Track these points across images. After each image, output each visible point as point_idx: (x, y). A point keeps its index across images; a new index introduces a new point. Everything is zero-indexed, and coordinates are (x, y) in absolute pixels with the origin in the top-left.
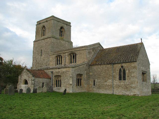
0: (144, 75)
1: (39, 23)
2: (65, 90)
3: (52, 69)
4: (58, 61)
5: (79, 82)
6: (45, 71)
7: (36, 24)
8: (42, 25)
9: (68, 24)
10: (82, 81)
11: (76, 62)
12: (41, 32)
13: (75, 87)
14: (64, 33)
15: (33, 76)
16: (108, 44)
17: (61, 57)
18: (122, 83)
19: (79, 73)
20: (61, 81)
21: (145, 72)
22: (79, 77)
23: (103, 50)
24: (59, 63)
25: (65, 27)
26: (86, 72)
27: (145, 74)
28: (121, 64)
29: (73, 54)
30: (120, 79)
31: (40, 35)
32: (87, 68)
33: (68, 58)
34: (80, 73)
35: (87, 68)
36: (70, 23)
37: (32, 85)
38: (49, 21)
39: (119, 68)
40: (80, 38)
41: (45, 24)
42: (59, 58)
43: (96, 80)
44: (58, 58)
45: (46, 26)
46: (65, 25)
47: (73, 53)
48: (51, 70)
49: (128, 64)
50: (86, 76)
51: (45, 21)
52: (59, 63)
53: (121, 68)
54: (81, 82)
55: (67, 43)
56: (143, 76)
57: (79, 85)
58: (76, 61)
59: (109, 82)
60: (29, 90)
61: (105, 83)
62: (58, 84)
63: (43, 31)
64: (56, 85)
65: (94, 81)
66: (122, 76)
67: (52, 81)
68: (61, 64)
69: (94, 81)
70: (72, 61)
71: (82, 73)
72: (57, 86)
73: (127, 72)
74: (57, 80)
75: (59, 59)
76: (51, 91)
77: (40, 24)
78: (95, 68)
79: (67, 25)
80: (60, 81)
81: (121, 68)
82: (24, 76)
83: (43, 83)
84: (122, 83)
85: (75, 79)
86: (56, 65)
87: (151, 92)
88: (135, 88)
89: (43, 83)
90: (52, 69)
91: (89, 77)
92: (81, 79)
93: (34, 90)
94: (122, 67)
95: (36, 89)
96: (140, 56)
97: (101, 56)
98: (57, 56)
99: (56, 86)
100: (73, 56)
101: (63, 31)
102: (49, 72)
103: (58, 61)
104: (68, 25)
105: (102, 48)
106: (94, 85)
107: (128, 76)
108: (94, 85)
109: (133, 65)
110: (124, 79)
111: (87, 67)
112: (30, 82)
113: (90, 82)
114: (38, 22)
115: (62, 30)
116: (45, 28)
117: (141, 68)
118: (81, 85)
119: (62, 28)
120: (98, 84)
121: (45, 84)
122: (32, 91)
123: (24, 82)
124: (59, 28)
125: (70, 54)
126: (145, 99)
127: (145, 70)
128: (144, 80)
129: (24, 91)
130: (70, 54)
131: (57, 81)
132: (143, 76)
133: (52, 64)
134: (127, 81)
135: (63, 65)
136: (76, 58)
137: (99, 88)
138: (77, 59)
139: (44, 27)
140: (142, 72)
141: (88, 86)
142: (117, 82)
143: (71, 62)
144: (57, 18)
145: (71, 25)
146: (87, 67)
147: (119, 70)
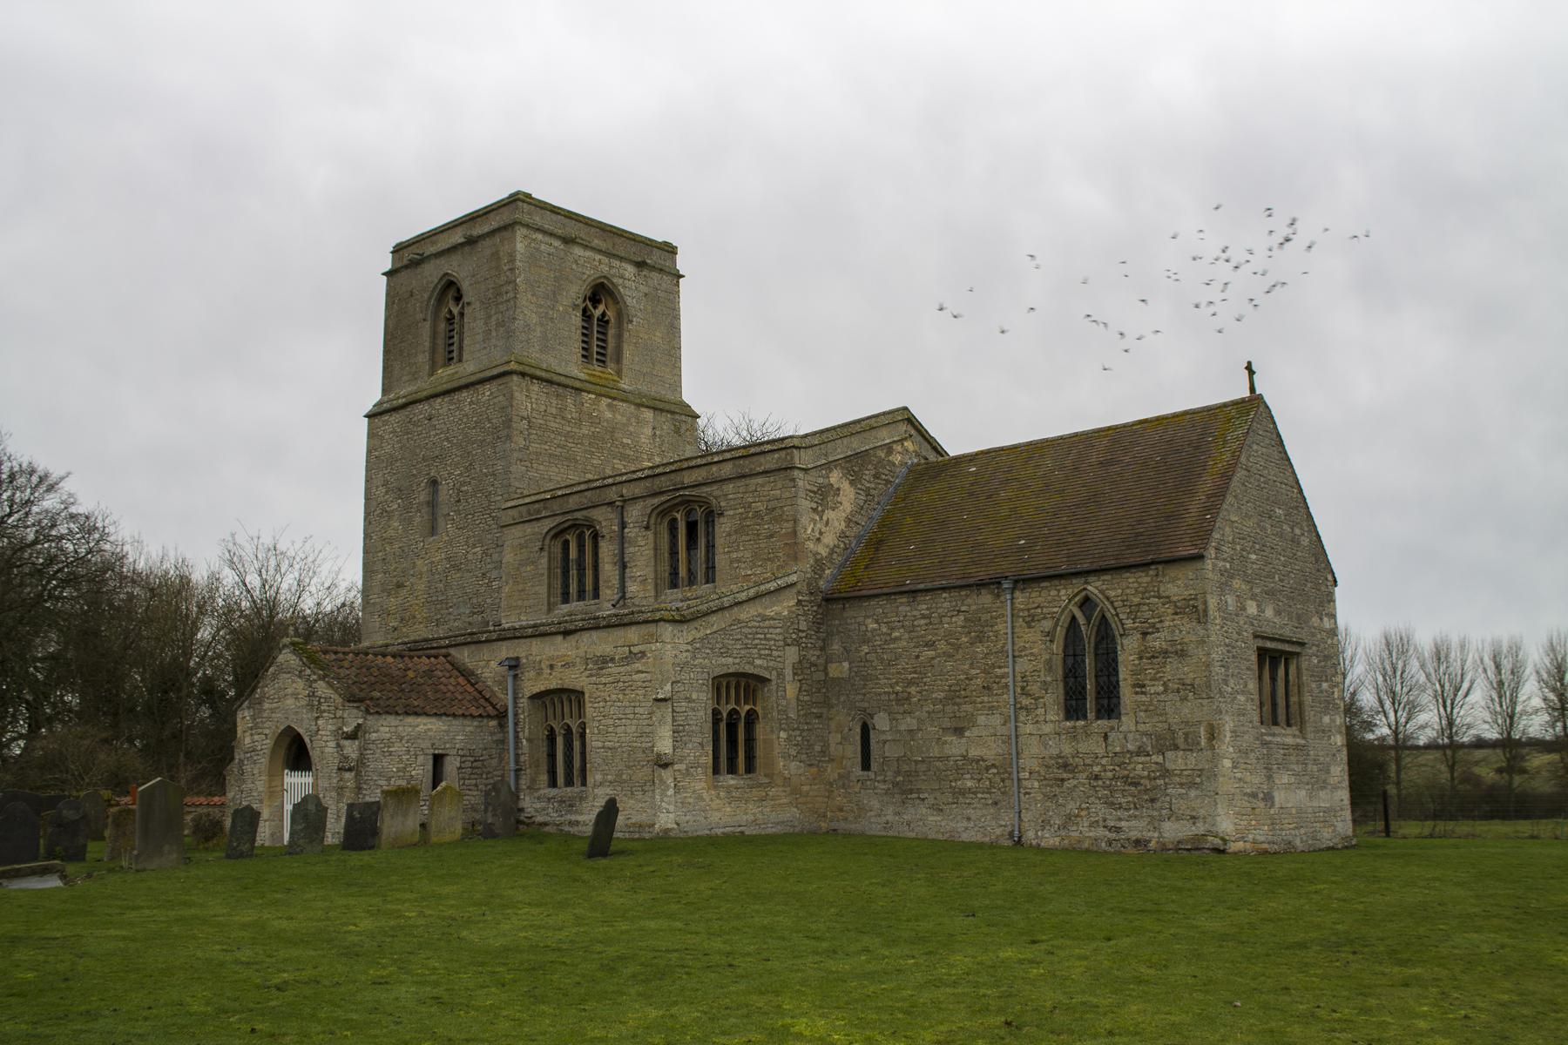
0: (1281, 672)
1: (410, 258)
2: (610, 810)
3: (515, 635)
4: (573, 572)
5: (735, 744)
6: (464, 656)
7: (388, 266)
8: (431, 273)
9: (655, 258)
10: (760, 731)
11: (710, 577)
12: (426, 330)
13: (699, 782)
14: (619, 337)
15: (352, 699)
16: (974, 417)
17: (596, 537)
18: (1091, 741)
19: (730, 664)
20: (583, 736)
21: (1287, 648)
22: (737, 702)
23: (936, 466)
24: (573, 588)
25: (630, 284)
26: (792, 654)
27: (1287, 667)
28: (1078, 583)
29: (698, 503)
30: (1073, 708)
31: (423, 358)
32: (803, 626)
33: (644, 552)
34: (749, 669)
35: (803, 626)
36: (670, 250)
37: (347, 775)
38: (487, 242)
39: (1065, 620)
40: (745, 375)
41: (461, 269)
42: (573, 545)
43: (881, 722)
44: (566, 544)
45: (465, 286)
46: (630, 270)
47: (687, 502)
48: (505, 651)
49: (1132, 580)
50: (791, 690)
51: (457, 237)
52: (573, 588)
53: (1081, 620)
54: (750, 741)
55: (648, 415)
56: (1273, 679)
57: (732, 770)
58: (711, 569)
59: (985, 738)
60: (309, 815)
61: (955, 747)
62: (565, 756)
63: (442, 326)
64: (544, 767)
65: (865, 731)
66: (1090, 685)
67: (517, 737)
68: (596, 595)
69: (865, 731)
70: (683, 572)
71: (758, 666)
72: (553, 783)
73: (1128, 650)
74: (552, 730)
75: (573, 554)
76: (502, 823)
77: (415, 264)
78: (869, 620)
79: (641, 265)
80: (576, 736)
81: (1081, 620)
82: (288, 697)
83: (438, 760)
84: (1094, 746)
85: (700, 718)
86: (550, 607)
87: (1348, 814)
88: (1193, 785)
89: (438, 760)
90: (515, 635)
91: (821, 691)
92: (751, 718)
93: (350, 817)
94: (1086, 603)
95: (373, 810)
96: (1234, 521)
97: (926, 517)
98: (558, 533)
99: (544, 778)
100: (692, 528)
101: (610, 314)
102: (488, 664)
103: (573, 572)
104: (653, 268)
105: (932, 457)
106: (866, 766)
107: (1140, 687)
108: (866, 766)
109: (1176, 584)
110: (1109, 707)
111: (805, 614)
112: (324, 747)
113: (834, 739)
114: (398, 250)
115: (601, 308)
116: (458, 299)
117: (1252, 608)
118: (750, 768)
119: (600, 292)
120: (892, 751)
121: (451, 766)
122: (335, 828)
123: (283, 752)
124: (575, 292)
125: (664, 512)
126: (1273, 867)
127: (1287, 632)
128: (1280, 709)
129: (276, 828)
130: (556, 536)
131: (551, 738)
132: (1273, 679)
133: (524, 595)
134: (1127, 722)
135: (606, 610)
136: (710, 547)
137: (904, 790)
138: (719, 549)
139: (450, 289)
140: (1260, 643)
141: (814, 770)
142: (1045, 731)
143: (674, 573)
144: (555, 210)
145: (682, 264)
146: (805, 614)
147: (1060, 632)
